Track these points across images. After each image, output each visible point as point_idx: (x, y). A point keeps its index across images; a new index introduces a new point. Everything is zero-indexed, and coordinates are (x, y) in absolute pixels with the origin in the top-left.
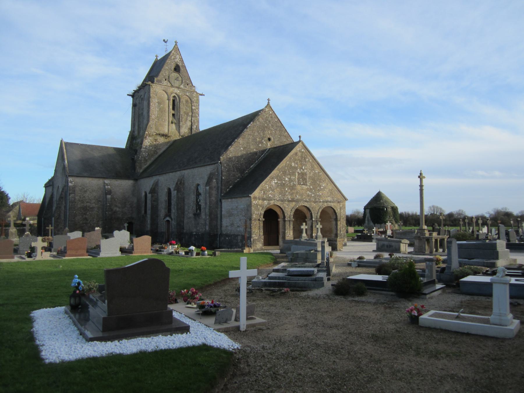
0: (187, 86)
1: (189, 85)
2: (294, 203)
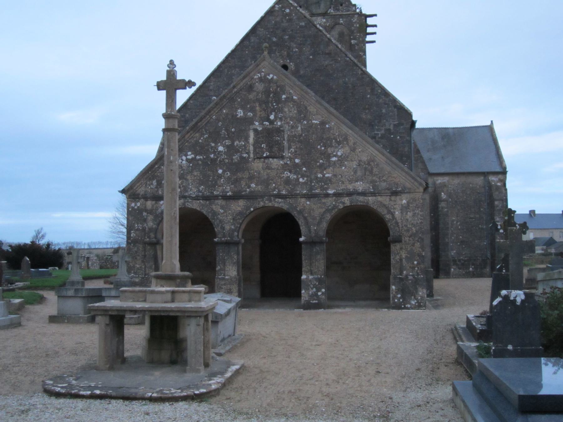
0: (341, 7)
1: (344, 5)
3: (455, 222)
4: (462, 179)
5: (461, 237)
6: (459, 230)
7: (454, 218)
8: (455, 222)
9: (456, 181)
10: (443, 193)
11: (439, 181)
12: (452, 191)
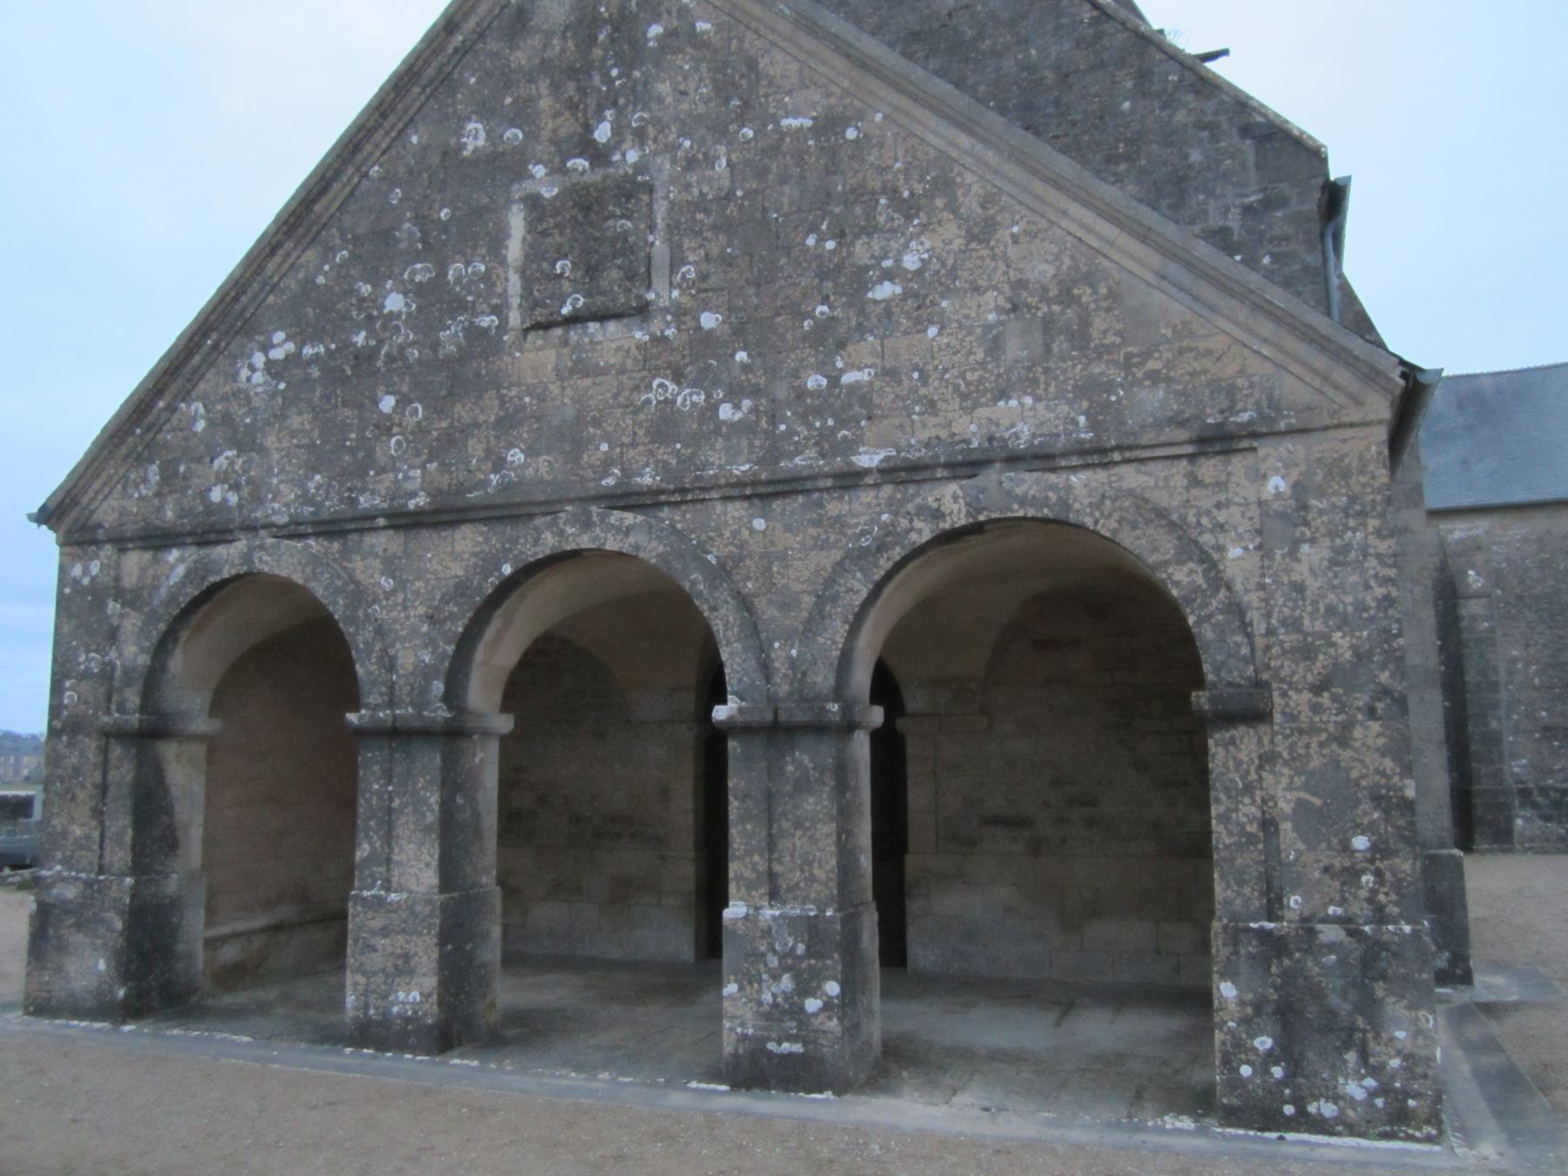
2: (467, 540)
3: (1519, 666)
4: (1540, 523)
5: (1544, 714)
6: (1536, 689)
7: (1515, 653)
8: (1519, 666)
9: (1517, 530)
10: (1471, 572)
11: (1457, 535)
12: (1504, 565)
